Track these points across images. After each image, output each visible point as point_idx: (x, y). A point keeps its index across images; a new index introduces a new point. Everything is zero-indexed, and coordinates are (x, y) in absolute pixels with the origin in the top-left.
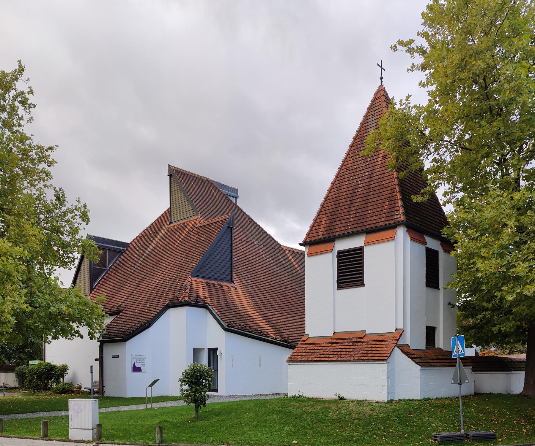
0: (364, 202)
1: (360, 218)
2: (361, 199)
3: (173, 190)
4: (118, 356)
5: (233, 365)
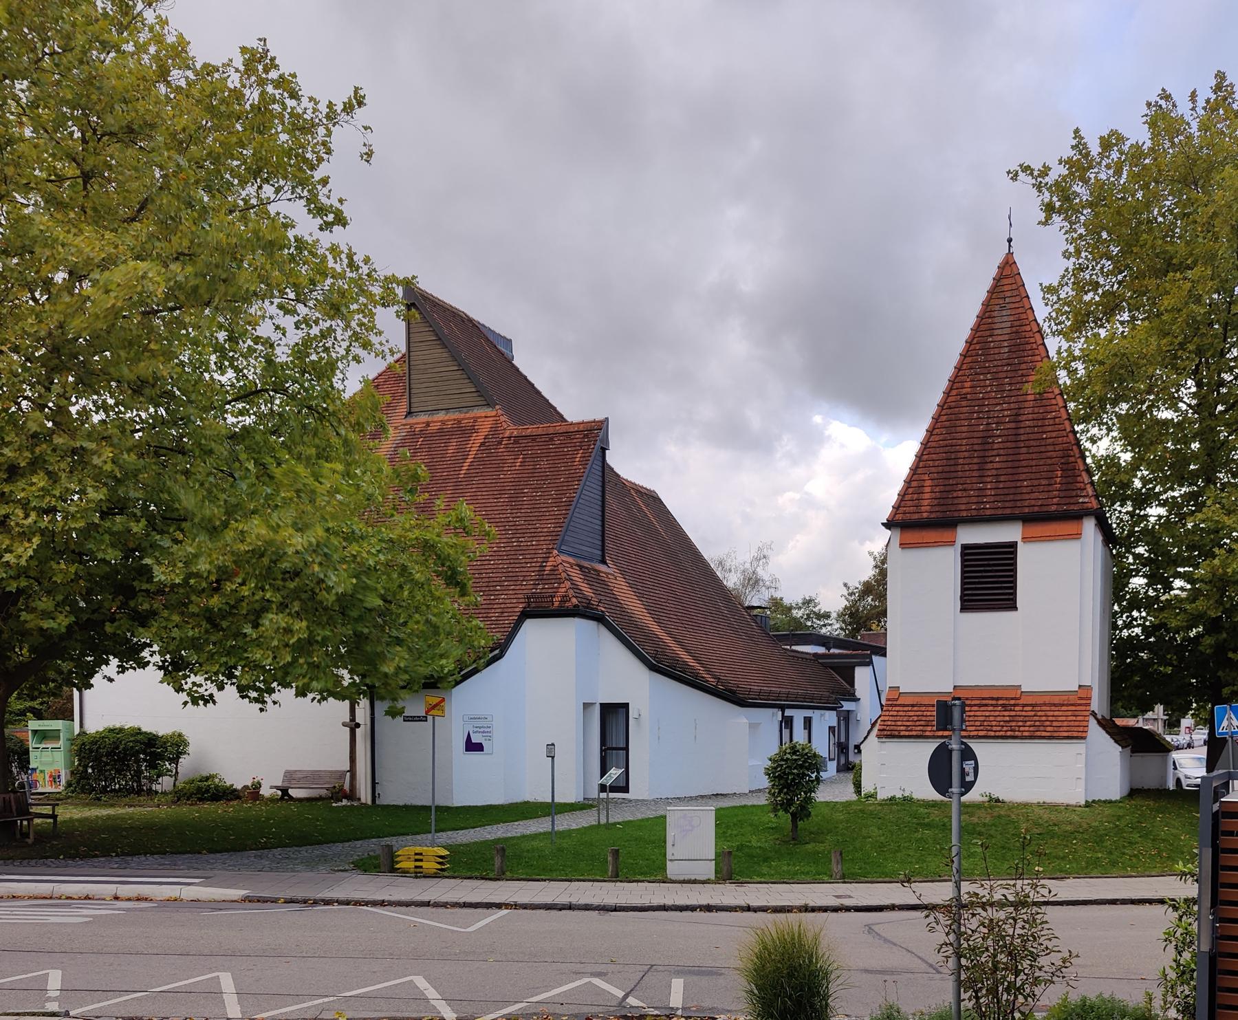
0: (1010, 464)
1: (1006, 491)
2: (1002, 458)
3: (414, 338)
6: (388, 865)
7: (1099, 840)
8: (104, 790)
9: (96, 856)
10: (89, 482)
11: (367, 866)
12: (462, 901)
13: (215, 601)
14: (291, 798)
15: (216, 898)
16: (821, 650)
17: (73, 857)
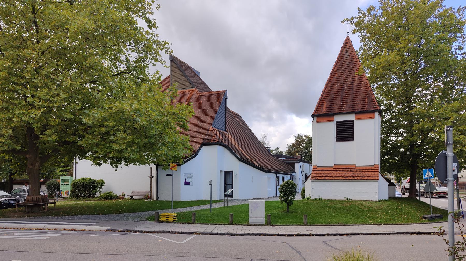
3: (173, 69)
6: (157, 219)
7: (387, 212)
8: (80, 196)
9: (65, 215)
10: (62, 91)
11: (150, 219)
12: (181, 231)
13: (103, 129)
14: (134, 199)
15: (98, 230)
16: (285, 159)
17: (57, 216)
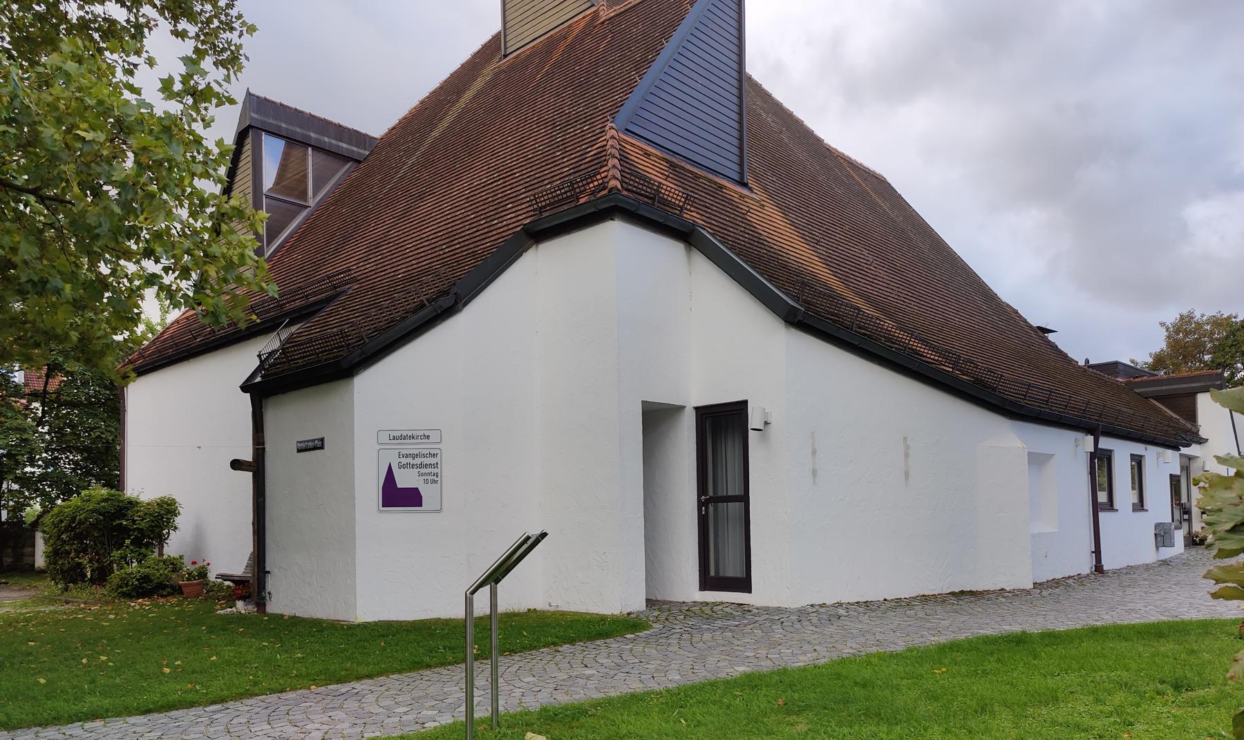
4: (319, 445)
5: (814, 473)
